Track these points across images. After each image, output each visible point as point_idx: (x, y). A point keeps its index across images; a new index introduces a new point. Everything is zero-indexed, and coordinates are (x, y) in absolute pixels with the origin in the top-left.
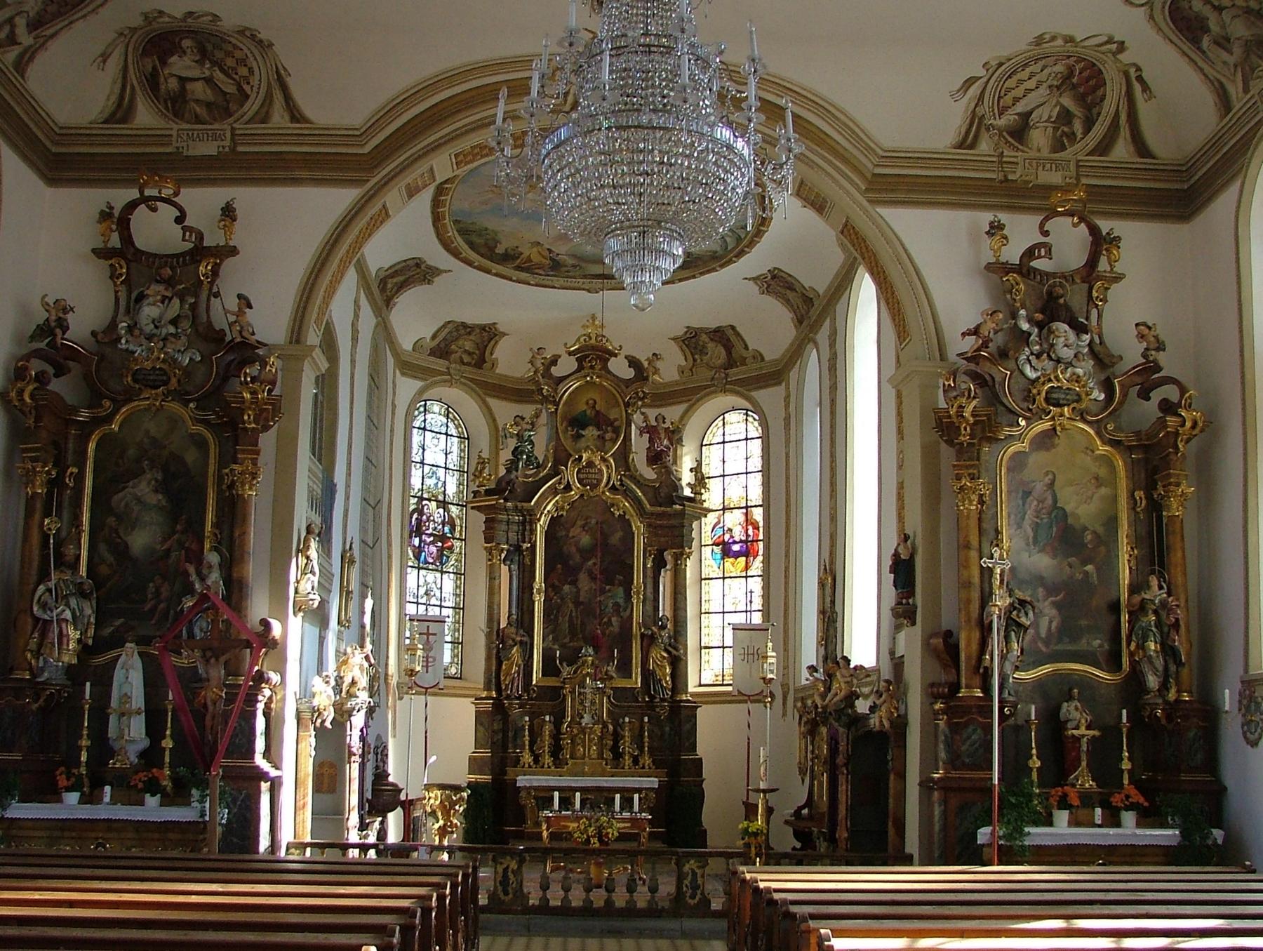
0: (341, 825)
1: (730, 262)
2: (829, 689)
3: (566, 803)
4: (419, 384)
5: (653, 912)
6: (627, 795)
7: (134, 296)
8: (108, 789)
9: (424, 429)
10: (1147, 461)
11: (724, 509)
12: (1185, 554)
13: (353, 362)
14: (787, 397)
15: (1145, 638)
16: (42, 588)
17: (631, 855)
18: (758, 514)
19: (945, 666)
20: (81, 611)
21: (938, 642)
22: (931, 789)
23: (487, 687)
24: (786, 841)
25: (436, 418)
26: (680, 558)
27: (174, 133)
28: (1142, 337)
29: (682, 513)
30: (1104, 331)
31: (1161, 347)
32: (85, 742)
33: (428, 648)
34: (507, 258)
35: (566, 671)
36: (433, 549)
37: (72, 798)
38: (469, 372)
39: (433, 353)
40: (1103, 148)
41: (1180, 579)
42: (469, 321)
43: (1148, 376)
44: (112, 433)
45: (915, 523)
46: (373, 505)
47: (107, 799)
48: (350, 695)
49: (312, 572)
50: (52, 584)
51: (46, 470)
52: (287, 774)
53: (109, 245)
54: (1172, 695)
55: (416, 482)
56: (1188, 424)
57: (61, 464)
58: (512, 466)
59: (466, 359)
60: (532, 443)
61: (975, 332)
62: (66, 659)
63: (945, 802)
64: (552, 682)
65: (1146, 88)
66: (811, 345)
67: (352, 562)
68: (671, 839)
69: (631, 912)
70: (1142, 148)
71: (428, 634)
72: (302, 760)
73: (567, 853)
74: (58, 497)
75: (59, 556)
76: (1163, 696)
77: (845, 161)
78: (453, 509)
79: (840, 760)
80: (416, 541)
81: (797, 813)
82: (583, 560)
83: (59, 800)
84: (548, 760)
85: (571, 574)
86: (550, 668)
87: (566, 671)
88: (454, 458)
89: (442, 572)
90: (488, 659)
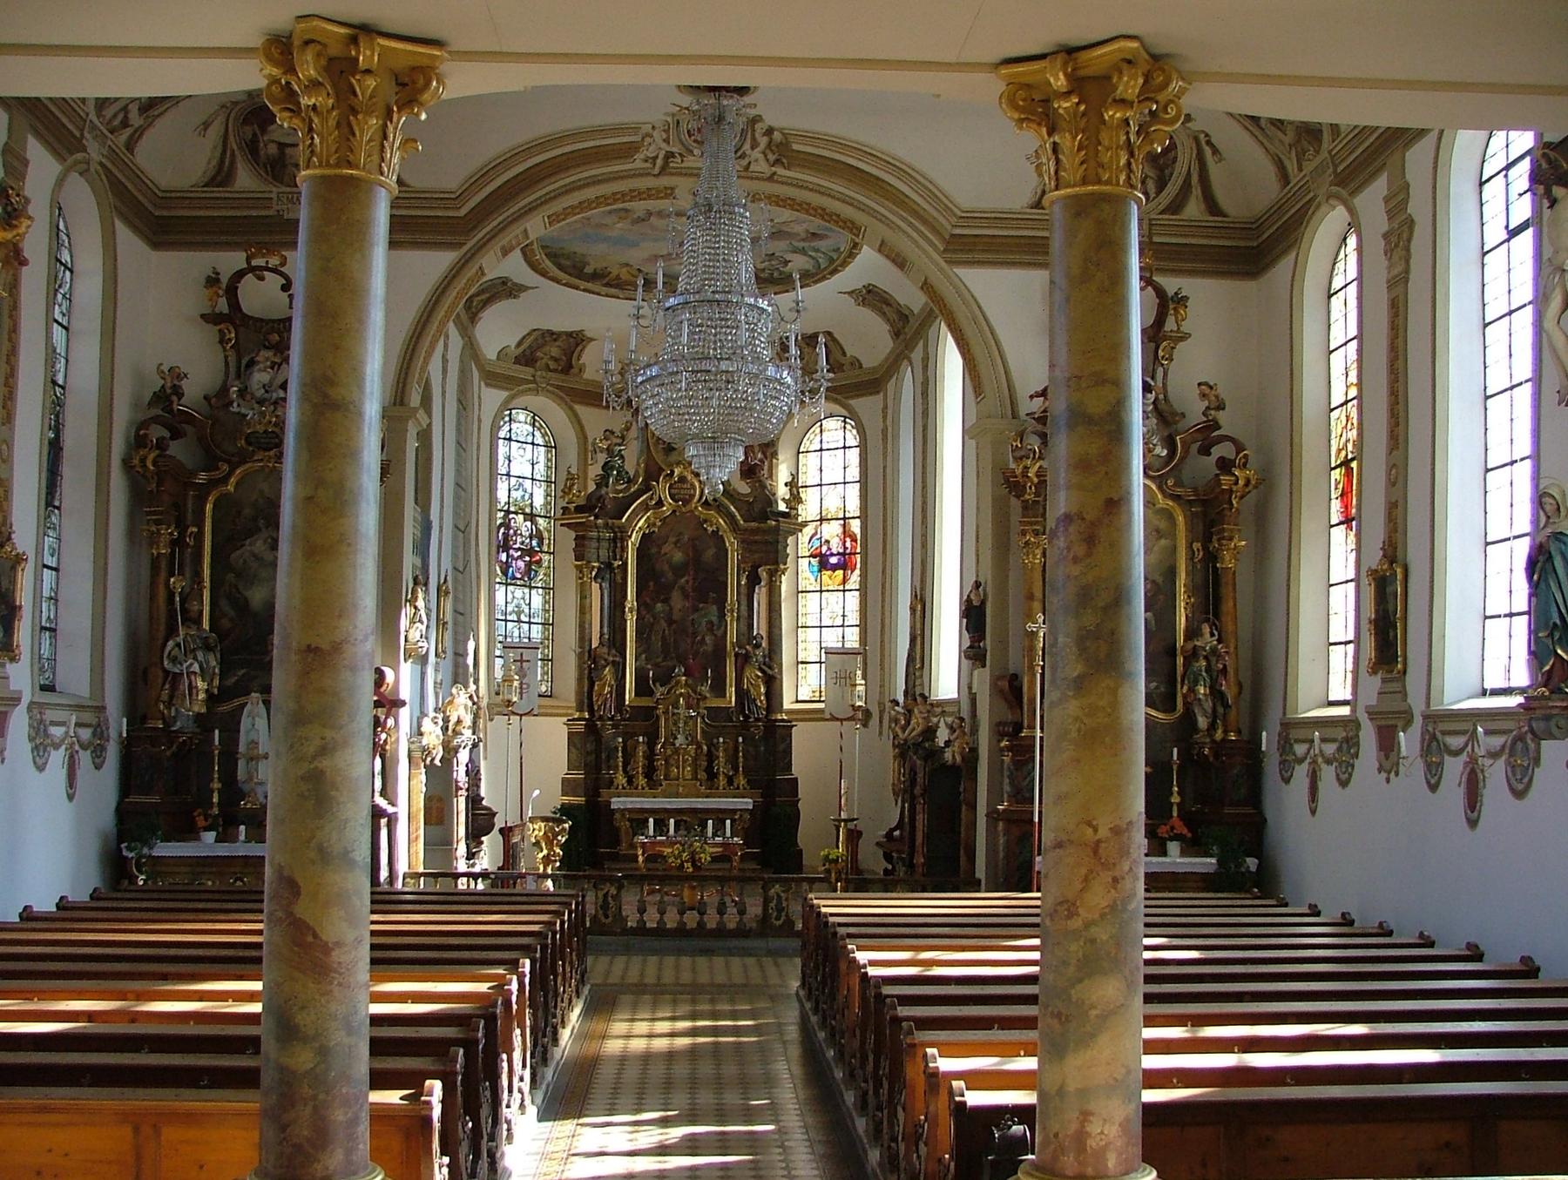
0: (450, 855)
1: (824, 278)
2: (908, 723)
3: (661, 826)
4: (505, 394)
5: (741, 932)
6: (720, 816)
7: (244, 362)
8: (242, 828)
9: (510, 439)
10: (1205, 514)
11: (821, 520)
12: (1238, 604)
13: (444, 393)
14: (885, 407)
15: (1196, 683)
16: (171, 644)
17: (722, 880)
18: (855, 526)
19: (1011, 707)
20: (207, 662)
21: (1005, 684)
22: (997, 820)
23: (580, 709)
24: (873, 861)
25: (521, 426)
26: (774, 575)
27: (274, 196)
28: (1204, 396)
29: (777, 529)
30: (1169, 389)
31: (1221, 407)
32: (216, 785)
33: (522, 673)
34: (595, 276)
35: (660, 691)
36: (521, 564)
37: (210, 837)
38: (557, 379)
39: (517, 361)
40: (1175, 207)
41: (1230, 628)
42: (555, 329)
43: (1208, 435)
44: (226, 495)
45: (987, 576)
46: (463, 530)
47: (242, 837)
48: (456, 733)
49: (421, 621)
50: (180, 639)
51: (168, 532)
52: (402, 810)
53: (217, 310)
54: (1219, 735)
55: (502, 495)
56: (1241, 482)
57: (181, 525)
58: (602, 482)
59: (552, 365)
60: (622, 457)
61: (1043, 393)
62: (196, 709)
63: (1007, 832)
64: (645, 702)
65: (1215, 151)
66: (905, 362)
67: (447, 593)
68: (765, 861)
69: (721, 932)
70: (1213, 207)
71: (521, 661)
72: (414, 796)
73: (663, 880)
74: (182, 555)
75: (184, 611)
76: (1211, 736)
77: (925, 222)
78: (541, 521)
79: (918, 790)
80: (504, 557)
81: (889, 835)
82: (676, 572)
83: (198, 839)
84: (642, 781)
85: (663, 593)
86: (642, 688)
87: (660, 691)
88: (540, 469)
89: (531, 588)
90: (580, 680)
